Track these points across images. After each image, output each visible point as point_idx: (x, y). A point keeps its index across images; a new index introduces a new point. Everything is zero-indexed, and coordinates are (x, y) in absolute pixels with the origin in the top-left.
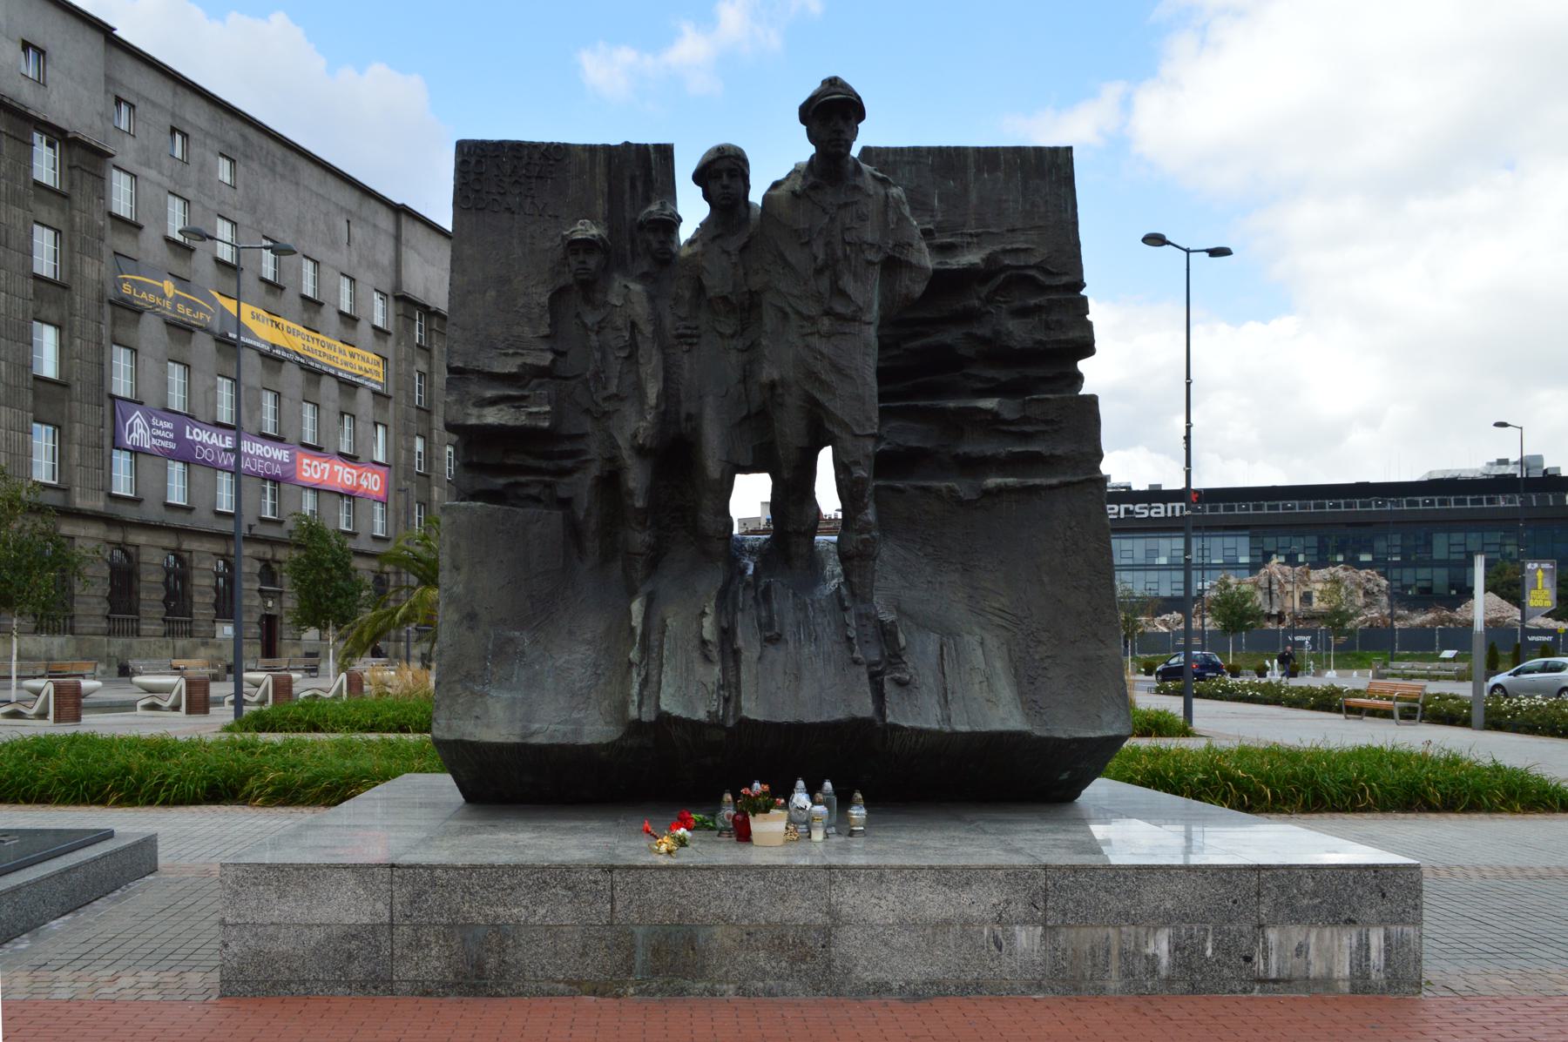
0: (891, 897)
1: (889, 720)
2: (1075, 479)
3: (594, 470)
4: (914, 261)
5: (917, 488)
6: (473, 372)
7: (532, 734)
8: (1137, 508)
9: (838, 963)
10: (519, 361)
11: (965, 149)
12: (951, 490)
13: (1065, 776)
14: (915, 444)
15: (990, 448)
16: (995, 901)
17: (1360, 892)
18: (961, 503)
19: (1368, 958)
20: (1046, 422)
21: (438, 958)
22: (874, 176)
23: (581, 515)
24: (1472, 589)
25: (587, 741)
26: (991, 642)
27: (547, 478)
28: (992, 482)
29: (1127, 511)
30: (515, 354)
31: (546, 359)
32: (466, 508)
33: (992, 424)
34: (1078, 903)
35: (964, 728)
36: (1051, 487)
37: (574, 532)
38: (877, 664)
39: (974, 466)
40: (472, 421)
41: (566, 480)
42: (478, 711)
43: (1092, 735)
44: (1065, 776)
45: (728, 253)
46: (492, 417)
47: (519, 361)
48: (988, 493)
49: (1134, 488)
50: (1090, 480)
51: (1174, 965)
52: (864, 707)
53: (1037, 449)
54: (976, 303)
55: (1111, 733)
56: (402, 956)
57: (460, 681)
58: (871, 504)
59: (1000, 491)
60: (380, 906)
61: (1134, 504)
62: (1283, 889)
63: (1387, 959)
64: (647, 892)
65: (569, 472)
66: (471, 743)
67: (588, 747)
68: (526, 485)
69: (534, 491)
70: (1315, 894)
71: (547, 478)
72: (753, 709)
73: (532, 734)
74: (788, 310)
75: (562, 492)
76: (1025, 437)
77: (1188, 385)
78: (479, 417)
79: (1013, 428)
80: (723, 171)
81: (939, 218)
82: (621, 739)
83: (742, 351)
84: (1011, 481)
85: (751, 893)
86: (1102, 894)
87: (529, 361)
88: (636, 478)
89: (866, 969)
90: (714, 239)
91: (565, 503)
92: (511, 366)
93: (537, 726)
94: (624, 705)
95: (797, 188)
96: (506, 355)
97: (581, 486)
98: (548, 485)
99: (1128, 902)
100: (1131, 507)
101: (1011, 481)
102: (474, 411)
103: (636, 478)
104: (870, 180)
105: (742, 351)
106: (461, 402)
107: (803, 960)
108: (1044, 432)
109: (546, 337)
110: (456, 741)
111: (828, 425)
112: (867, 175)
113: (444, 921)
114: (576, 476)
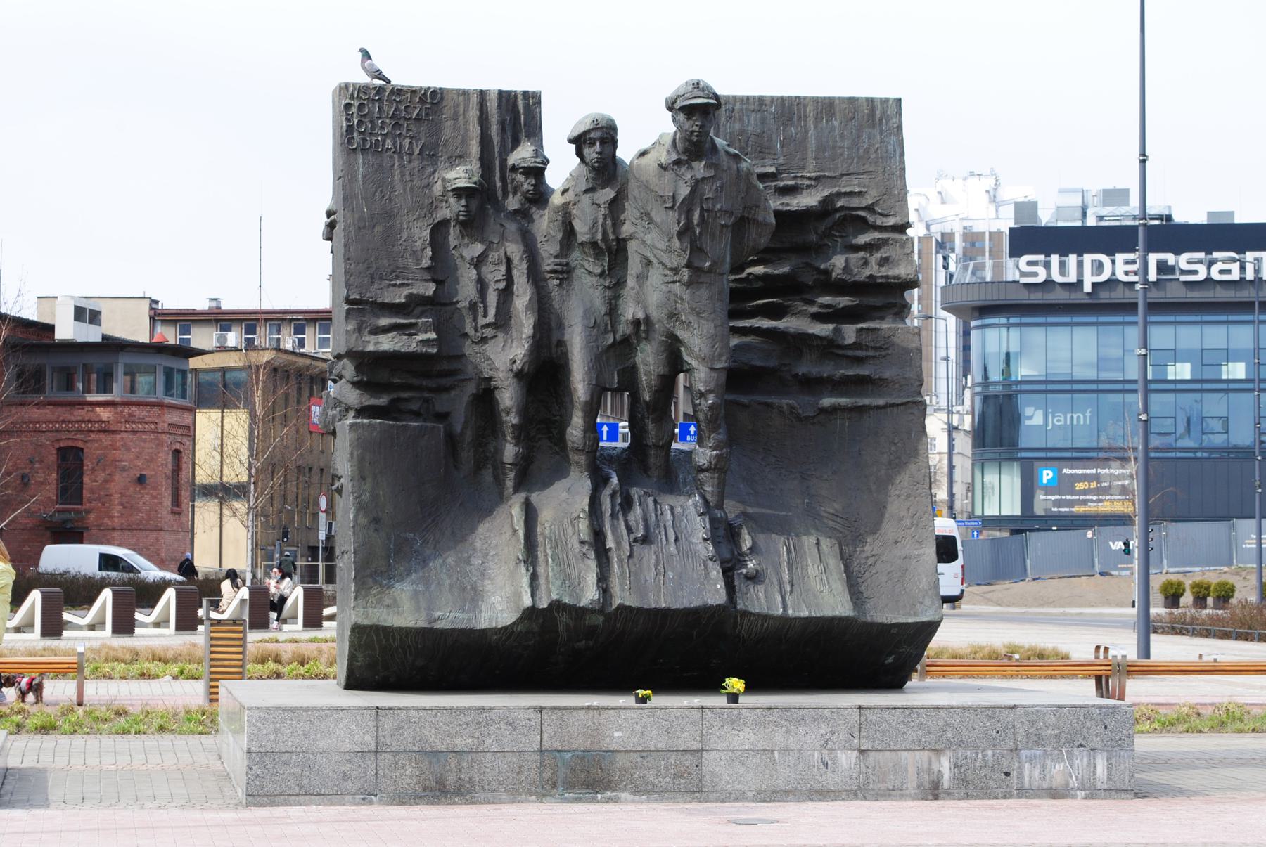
0: (747, 730)
1: (740, 606)
2: (899, 401)
3: (471, 388)
4: (760, 219)
5: (760, 404)
6: (367, 302)
7: (435, 621)
8: (1183, 260)
9: (707, 779)
10: (406, 291)
11: (799, 102)
12: (792, 407)
13: (890, 660)
14: (758, 363)
15: (827, 369)
16: (823, 732)
17: (1088, 725)
18: (799, 418)
19: (1094, 773)
20: (875, 348)
21: (411, 777)
22: (727, 152)
23: (458, 428)
24: (156, 601)
25: (483, 627)
26: (826, 544)
27: (426, 395)
28: (827, 402)
29: (1162, 267)
30: (402, 285)
31: (430, 289)
32: (370, 424)
33: (829, 348)
34: (884, 733)
35: (804, 613)
36: (878, 407)
37: (452, 441)
38: (728, 562)
39: (813, 385)
40: (371, 348)
41: (445, 396)
42: (387, 601)
43: (910, 620)
44: (890, 660)
45: (599, 205)
46: (387, 343)
47: (406, 291)
48: (823, 411)
49: (1178, 218)
50: (915, 403)
51: (954, 779)
52: (715, 594)
53: (867, 373)
54: (814, 238)
55: (925, 619)
56: (384, 775)
57: (371, 576)
58: (723, 424)
59: (834, 409)
60: (368, 738)
61: (1178, 252)
62: (1032, 722)
63: (1109, 774)
64: (567, 726)
65: (447, 389)
66: (384, 628)
67: (483, 632)
68: (407, 400)
69: (414, 406)
70: (1056, 726)
71: (426, 395)
72: (622, 596)
73: (435, 621)
74: (652, 258)
75: (439, 408)
76: (859, 361)
77: (1143, 162)
78: (377, 343)
79: (850, 353)
80: (597, 141)
81: (781, 161)
82: (514, 624)
83: (609, 288)
84: (843, 401)
85: (644, 726)
86: (901, 726)
87: (415, 291)
88: (508, 397)
89: (728, 783)
90: (586, 191)
91: (443, 417)
92: (399, 297)
93: (439, 613)
94: (518, 595)
95: (663, 161)
96: (395, 285)
97: (459, 404)
98: (427, 401)
99: (920, 733)
100: (1170, 258)
101: (843, 401)
102: (372, 338)
103: (508, 397)
104: (724, 157)
105: (609, 288)
106: (359, 330)
107: (682, 776)
108: (874, 357)
109: (428, 269)
110: (371, 627)
111: (686, 357)
112: (722, 153)
113: (416, 749)
114: (453, 393)
